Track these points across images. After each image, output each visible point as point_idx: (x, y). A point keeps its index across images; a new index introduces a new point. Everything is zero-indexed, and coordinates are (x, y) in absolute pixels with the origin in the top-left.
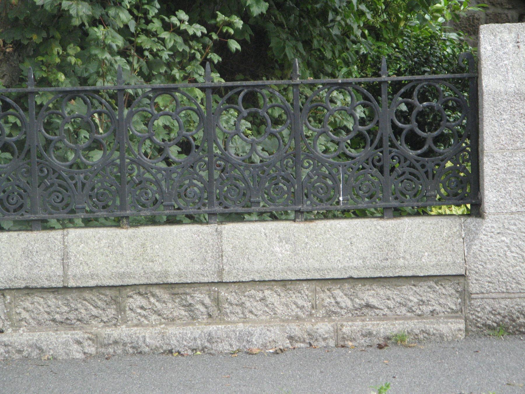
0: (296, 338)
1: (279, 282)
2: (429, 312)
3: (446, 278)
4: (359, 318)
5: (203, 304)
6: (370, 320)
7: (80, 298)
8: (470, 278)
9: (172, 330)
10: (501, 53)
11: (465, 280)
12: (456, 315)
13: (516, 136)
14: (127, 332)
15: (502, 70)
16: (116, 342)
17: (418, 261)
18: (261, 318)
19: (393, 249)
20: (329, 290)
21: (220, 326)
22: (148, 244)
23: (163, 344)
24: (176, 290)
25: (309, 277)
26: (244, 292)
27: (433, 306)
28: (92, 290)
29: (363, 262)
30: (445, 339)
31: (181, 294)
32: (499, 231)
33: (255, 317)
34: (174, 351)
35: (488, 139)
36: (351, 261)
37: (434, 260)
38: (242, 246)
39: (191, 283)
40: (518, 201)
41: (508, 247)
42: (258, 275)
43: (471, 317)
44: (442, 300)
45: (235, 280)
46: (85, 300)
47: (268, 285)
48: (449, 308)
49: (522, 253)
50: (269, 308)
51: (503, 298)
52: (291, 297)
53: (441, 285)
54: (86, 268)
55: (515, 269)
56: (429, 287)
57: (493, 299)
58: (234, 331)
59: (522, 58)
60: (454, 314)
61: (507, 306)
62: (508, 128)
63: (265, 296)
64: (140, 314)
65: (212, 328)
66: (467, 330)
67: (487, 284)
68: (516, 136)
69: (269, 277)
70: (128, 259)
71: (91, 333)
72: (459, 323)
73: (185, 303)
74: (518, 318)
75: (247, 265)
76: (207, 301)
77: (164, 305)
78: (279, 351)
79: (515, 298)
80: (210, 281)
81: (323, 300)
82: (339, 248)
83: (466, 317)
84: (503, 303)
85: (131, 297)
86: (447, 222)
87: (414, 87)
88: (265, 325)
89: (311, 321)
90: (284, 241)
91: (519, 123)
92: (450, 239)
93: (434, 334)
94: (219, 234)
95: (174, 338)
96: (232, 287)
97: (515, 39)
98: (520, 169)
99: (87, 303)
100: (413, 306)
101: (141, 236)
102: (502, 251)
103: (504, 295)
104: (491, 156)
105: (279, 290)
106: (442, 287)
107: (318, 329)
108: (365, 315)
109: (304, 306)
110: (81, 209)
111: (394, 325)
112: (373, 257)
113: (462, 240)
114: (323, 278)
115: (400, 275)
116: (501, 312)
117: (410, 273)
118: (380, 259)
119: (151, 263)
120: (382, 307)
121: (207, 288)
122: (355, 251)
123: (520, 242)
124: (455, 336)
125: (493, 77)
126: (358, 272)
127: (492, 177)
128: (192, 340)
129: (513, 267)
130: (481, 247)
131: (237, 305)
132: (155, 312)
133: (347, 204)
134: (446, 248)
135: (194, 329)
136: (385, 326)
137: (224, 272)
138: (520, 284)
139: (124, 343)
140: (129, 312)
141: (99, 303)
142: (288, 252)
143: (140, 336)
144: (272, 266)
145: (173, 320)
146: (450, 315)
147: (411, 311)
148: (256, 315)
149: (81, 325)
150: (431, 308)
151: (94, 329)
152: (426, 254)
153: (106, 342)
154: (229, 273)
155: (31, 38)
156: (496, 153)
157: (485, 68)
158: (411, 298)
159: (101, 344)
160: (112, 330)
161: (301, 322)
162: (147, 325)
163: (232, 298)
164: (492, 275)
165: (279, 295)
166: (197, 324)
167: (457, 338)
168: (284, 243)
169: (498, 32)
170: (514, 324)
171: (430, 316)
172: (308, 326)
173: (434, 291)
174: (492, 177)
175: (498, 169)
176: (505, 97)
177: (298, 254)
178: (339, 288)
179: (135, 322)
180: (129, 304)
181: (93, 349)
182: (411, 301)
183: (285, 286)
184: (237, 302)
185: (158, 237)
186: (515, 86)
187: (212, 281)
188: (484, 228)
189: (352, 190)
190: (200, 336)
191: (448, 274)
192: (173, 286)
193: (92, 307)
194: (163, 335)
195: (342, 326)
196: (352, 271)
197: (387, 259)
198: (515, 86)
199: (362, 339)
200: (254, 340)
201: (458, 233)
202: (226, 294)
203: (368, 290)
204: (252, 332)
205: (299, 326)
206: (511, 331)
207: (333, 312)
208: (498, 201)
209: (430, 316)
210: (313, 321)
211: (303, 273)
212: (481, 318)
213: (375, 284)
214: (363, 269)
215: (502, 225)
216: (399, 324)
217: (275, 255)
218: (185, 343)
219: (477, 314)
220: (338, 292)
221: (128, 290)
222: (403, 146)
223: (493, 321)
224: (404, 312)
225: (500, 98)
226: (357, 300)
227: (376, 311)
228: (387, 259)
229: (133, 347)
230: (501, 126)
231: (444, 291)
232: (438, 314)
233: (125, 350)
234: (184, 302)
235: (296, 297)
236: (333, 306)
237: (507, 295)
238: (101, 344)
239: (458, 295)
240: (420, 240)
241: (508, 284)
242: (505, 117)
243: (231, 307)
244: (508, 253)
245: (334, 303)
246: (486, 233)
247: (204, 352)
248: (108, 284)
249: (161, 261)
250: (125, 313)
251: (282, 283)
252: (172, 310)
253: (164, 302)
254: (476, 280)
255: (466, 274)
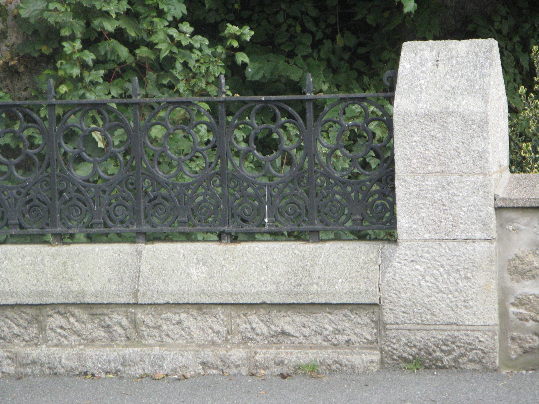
0: (209, 364)
1: (195, 305)
2: (344, 342)
3: (360, 306)
4: (275, 345)
5: (121, 326)
6: (286, 348)
7: (3, 316)
8: (385, 307)
9: (90, 352)
10: (419, 72)
11: (380, 309)
12: (372, 346)
13: (428, 159)
14: (46, 352)
15: (416, 89)
16: (34, 362)
17: (331, 288)
18: (178, 342)
19: (307, 275)
20: (245, 315)
21: (136, 349)
22: (69, 263)
23: (79, 366)
24: (94, 311)
25: (222, 301)
26: (160, 315)
27: (349, 335)
28: (13, 308)
29: (277, 287)
30: (357, 371)
31: (100, 315)
32: (412, 259)
33: (172, 341)
34: (89, 373)
35: (399, 162)
36: (265, 285)
37: (347, 287)
38: (160, 267)
39: (107, 304)
40: (431, 228)
41: (422, 275)
42: (173, 298)
43: (386, 348)
44: (358, 330)
45: (150, 302)
46: (7, 318)
47: (183, 308)
48: (365, 338)
49: (437, 283)
50: (186, 332)
51: (418, 330)
52: (207, 321)
53: (356, 314)
54: (7, 285)
55: (430, 299)
56: (345, 315)
57: (409, 330)
58: (149, 355)
59: (438, 77)
60: (370, 345)
61: (423, 338)
62: (419, 150)
63: (180, 320)
64: (59, 334)
65: (128, 351)
66: (382, 362)
67: (402, 314)
68: (428, 159)
69: (183, 299)
70: (48, 277)
71: (10, 352)
72: (373, 354)
73: (104, 324)
74: (434, 351)
75: (162, 287)
76: (125, 322)
77: (83, 325)
78: (182, 378)
79: (431, 330)
80: (126, 302)
81: (239, 325)
82: (255, 272)
83: (381, 348)
84: (419, 335)
85: (51, 316)
86: (365, 248)
87: (254, 106)
88: (178, 348)
89: (227, 347)
90: (201, 263)
91: (431, 146)
92: (366, 266)
93: (346, 365)
94: (138, 254)
95: (90, 360)
96: (149, 310)
97: (435, 58)
98: (432, 194)
99: (9, 321)
100: (328, 335)
101: (64, 254)
102: (416, 279)
103: (419, 327)
104: (403, 179)
105: (195, 314)
106: (357, 316)
107: (231, 356)
108: (281, 343)
109: (219, 332)
110: (14, 225)
111: (308, 354)
112: (287, 282)
113: (378, 267)
114: (236, 302)
115: (313, 302)
116: (417, 344)
117: (323, 300)
118: (293, 284)
119: (69, 283)
120: (298, 335)
121: (124, 309)
122: (269, 276)
123: (435, 271)
124: (366, 369)
125: (405, 98)
126: (271, 298)
127: (404, 202)
128: (106, 363)
129: (428, 298)
130: (394, 275)
131: (154, 328)
132: (75, 332)
133: (272, 226)
134: (361, 275)
135: (111, 351)
136: (299, 355)
137: (139, 293)
138: (435, 316)
139: (42, 364)
140: (49, 332)
141: (21, 321)
142: (204, 275)
143: (57, 357)
144: (186, 289)
145: (93, 341)
146: (366, 345)
147: (326, 340)
148: (173, 339)
149: (4, 344)
150: (346, 338)
151: (16, 347)
152: (340, 281)
153: (25, 362)
154: (144, 294)
155: (41, 50)
156: (407, 176)
157: (400, 87)
158: (326, 326)
159: (20, 363)
160: (32, 350)
161: (217, 348)
162: (67, 345)
163: (149, 320)
164: (406, 305)
165: (196, 319)
166: (115, 346)
167: (369, 370)
168: (201, 264)
169: (420, 50)
170: (430, 357)
171: (345, 345)
172: (222, 352)
173: (349, 320)
174: (404, 202)
175: (410, 194)
176: (416, 118)
177: (213, 277)
178: (255, 314)
179: (55, 342)
180: (49, 323)
181: (12, 368)
182: (326, 330)
183: (200, 309)
184: (153, 325)
185: (80, 255)
186: (426, 107)
187: (128, 302)
188: (397, 255)
189: (277, 213)
190: (115, 360)
191: (361, 302)
192: (91, 306)
193: (14, 325)
194: (79, 356)
195: (256, 353)
196: (266, 296)
197: (301, 285)
198: (426, 107)
199: (275, 368)
200: (165, 365)
201: (374, 260)
202: (143, 317)
203: (284, 316)
204: (165, 356)
205: (213, 351)
206: (427, 365)
207: (249, 338)
208: (411, 227)
209: (345, 345)
210: (229, 347)
211: (216, 296)
212: (396, 350)
213: (290, 311)
214: (276, 294)
215: (415, 253)
216: (313, 354)
217: (191, 277)
218: (100, 366)
219: (392, 345)
220: (254, 318)
221: (48, 309)
222: (71, 172)
223: (409, 354)
224: (320, 341)
225: (410, 120)
226: (273, 327)
227: (291, 338)
228: (301, 285)
229: (50, 368)
230: (412, 148)
231: (359, 320)
232: (353, 344)
233: (42, 371)
234: (103, 323)
235: (212, 321)
236: (249, 332)
237: (422, 327)
238: (20, 363)
239: (373, 325)
240: (336, 266)
241: (423, 315)
242: (415, 139)
243: (148, 330)
244: (423, 283)
245: (250, 329)
246: (400, 261)
247: (117, 375)
248: (27, 302)
249: (79, 280)
250: (45, 332)
251: (197, 306)
252: (92, 331)
253: (83, 322)
254: (391, 309)
255: (380, 302)
